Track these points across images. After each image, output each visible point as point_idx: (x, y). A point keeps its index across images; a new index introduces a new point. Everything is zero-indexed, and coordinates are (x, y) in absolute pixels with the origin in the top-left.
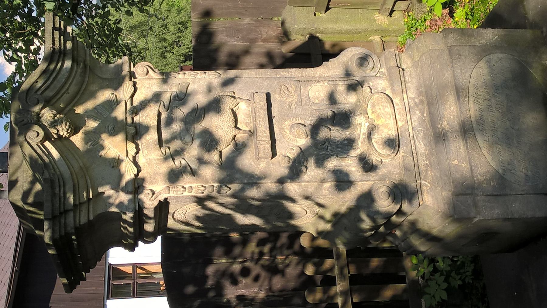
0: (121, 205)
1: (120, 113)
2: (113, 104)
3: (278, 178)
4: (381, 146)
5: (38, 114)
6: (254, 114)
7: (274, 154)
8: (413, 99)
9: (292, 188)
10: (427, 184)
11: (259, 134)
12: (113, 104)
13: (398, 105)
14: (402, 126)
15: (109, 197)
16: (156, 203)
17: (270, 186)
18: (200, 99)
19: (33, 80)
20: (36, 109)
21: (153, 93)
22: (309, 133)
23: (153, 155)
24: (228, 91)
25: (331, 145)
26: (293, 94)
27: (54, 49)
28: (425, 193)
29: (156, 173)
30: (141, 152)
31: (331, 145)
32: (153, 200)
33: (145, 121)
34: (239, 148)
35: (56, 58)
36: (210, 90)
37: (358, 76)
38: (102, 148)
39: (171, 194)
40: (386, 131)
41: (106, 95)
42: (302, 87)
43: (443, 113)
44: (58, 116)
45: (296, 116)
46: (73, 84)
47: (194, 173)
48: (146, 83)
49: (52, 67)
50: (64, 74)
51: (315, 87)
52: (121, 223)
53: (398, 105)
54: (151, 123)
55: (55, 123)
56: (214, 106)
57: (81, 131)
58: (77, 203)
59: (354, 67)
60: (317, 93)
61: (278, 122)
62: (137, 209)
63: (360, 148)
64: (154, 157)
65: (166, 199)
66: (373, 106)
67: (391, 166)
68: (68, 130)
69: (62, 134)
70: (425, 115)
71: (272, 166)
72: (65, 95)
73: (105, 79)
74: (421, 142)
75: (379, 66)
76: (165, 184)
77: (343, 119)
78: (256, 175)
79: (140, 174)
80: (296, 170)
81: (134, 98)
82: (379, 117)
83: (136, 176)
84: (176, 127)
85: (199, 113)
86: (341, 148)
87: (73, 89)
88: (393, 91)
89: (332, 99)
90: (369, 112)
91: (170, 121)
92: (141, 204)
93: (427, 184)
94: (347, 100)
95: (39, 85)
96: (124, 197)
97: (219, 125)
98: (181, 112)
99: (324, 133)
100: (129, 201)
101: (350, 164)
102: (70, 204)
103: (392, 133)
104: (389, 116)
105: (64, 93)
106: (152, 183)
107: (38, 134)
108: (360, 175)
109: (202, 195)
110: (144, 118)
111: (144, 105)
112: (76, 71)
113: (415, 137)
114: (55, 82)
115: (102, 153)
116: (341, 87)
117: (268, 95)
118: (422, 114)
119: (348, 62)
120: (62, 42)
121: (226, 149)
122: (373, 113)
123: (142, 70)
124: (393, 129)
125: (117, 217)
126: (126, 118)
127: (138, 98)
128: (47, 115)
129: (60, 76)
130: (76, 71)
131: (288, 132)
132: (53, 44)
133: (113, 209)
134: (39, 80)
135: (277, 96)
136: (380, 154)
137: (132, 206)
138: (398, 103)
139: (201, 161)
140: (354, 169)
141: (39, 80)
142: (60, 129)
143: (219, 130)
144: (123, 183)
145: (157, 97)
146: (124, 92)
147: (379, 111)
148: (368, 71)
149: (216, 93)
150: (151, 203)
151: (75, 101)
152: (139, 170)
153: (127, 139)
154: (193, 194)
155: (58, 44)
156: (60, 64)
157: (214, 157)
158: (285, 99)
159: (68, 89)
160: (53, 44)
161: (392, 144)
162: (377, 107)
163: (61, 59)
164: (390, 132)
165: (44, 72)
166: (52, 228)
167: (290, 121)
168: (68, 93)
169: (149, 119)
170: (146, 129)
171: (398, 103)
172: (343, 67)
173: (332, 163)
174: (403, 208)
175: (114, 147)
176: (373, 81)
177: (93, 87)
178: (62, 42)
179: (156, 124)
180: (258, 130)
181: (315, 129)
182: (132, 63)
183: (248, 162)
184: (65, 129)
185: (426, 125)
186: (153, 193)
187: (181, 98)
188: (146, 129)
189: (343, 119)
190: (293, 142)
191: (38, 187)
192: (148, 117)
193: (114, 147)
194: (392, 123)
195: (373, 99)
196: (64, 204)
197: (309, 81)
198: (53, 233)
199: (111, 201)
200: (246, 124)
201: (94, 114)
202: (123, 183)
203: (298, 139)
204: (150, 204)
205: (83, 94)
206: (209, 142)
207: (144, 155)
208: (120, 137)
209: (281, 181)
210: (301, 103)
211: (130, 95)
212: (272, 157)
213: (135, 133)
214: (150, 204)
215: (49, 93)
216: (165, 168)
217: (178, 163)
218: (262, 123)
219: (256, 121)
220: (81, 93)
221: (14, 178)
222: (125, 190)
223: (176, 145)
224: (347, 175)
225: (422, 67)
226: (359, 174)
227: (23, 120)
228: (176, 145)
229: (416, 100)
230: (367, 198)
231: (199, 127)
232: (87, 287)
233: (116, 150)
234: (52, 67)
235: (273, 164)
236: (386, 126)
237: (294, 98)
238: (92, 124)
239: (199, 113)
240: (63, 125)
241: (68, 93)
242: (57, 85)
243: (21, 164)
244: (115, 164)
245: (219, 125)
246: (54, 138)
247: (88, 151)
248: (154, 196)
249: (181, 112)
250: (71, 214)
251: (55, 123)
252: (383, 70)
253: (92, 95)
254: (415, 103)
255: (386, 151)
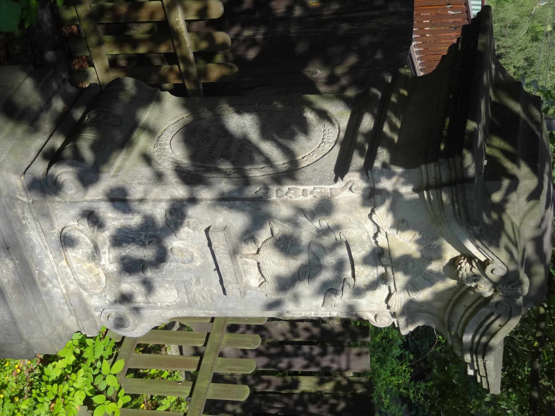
0: (390, 175)
1: (401, 279)
2: (412, 287)
3: (199, 204)
4: (81, 240)
5: (495, 291)
6: (238, 275)
7: (207, 230)
8: (54, 286)
9: (180, 191)
10: (21, 198)
11: (228, 256)
12: (412, 287)
13: (71, 282)
14: (60, 261)
15: (405, 184)
16: (347, 177)
17: (205, 194)
18: (305, 288)
19: (505, 328)
20: (497, 299)
21: (366, 298)
22: (169, 254)
23: (355, 234)
24: (274, 297)
25: (141, 241)
26: (196, 293)
27: (483, 358)
28: (21, 188)
29: (350, 212)
30: (372, 235)
31: (141, 241)
32: (350, 181)
33: (369, 270)
34: (248, 236)
35: (480, 348)
36: (296, 298)
37: (123, 309)
38: (418, 242)
39: (328, 187)
40: (79, 256)
41: (423, 295)
42: (187, 301)
43: (15, 276)
44: (473, 286)
45: (189, 270)
46: (460, 315)
47: (300, 210)
48: (375, 308)
49: (484, 339)
50: (473, 324)
51: (171, 301)
52: (396, 138)
53: (71, 282)
54: (362, 269)
55: (475, 278)
56: (286, 284)
57: (447, 261)
58: (438, 191)
59: (131, 318)
60: (168, 294)
61: (209, 264)
62: (369, 172)
63: (105, 236)
64: (353, 232)
65: (336, 180)
66: (99, 282)
67: (65, 216)
68: (460, 269)
69: (468, 264)
70: (37, 272)
71: (209, 219)
72: (469, 304)
73: (425, 312)
74: (37, 243)
75: (102, 318)
76: (337, 200)
77: (130, 267)
78: (226, 210)
79: (369, 212)
80: (177, 213)
81: (387, 292)
82: (90, 270)
83: (373, 211)
84: (329, 260)
85: (306, 273)
86: (129, 237)
87: (460, 310)
88: (80, 296)
89: (148, 286)
90: (102, 275)
91: (339, 266)
92: (365, 177)
93: (21, 198)
94: (130, 284)
95: (498, 323)
96: (386, 184)
97: (278, 265)
98: (326, 275)
99: (146, 253)
100: (379, 181)
101: (114, 220)
102: (446, 192)
103: (71, 253)
104: (79, 271)
105: (469, 307)
106: (353, 201)
107: (492, 272)
108: (101, 208)
109: (290, 186)
110: (372, 274)
111: (373, 286)
112: (458, 328)
113: (44, 248)
114: (480, 322)
115: (417, 236)
116: (140, 299)
117: (208, 334)
118: (40, 273)
119: (139, 322)
120: (475, 363)
121: (264, 235)
122: (98, 275)
123: (382, 321)
124: (70, 257)
125: (394, 161)
126: (393, 274)
127: (382, 291)
128: (485, 289)
129: (475, 328)
130: (458, 328)
131: (195, 254)
132: (485, 364)
133: (399, 170)
134: (499, 328)
135: (215, 291)
136: (81, 231)
137: (376, 176)
138: (70, 285)
139: (293, 222)
140: (110, 215)
141: (499, 328)
142: (468, 271)
143: (277, 261)
144: (388, 203)
145: (358, 292)
146: (400, 299)
147: (92, 276)
148: (113, 314)
149: (286, 296)
150: (352, 178)
151: (458, 294)
152: (370, 216)
153: (389, 251)
154: (301, 188)
155: (479, 363)
156: (477, 338)
157: (279, 229)
158: (206, 289)
159: (466, 311)
160: (485, 364)
161: (67, 241)
162: (94, 280)
163: (474, 346)
164: (74, 254)
165: (493, 335)
166: (464, 170)
167: (195, 266)
168: (465, 306)
169: (366, 273)
170: (366, 261)
171: (70, 285)
172: (144, 317)
173: (135, 220)
174: (46, 166)
175: (405, 243)
176: (105, 305)
177: (439, 304)
178: (475, 363)
179: (356, 268)
180: (229, 260)
181: (161, 258)
182: (397, 326)
183: (237, 221)
184: (463, 270)
185: (33, 261)
186: (350, 189)
187: (329, 290)
188: (366, 261)
189: (130, 267)
190: (188, 243)
191: (497, 197)
192: (366, 274)
193: (405, 243)
194: (74, 264)
195: (101, 288)
196: (452, 193)
197: (181, 305)
198: (462, 164)
199: (402, 180)
200: (247, 263)
201: (431, 279)
202: (388, 203)
203: (182, 246)
204: (354, 178)
205: (450, 300)
206: (286, 245)
207: (366, 234)
208: (398, 253)
209: (193, 200)
210: (186, 284)
211: (393, 297)
212: (209, 228)
213: (378, 256)
214: (354, 178)
215: (485, 311)
216: (338, 217)
217: (325, 223)
218: (227, 268)
219: (234, 269)
220: (452, 303)
221: (532, 203)
222: (384, 193)
223: (327, 241)
224: (117, 209)
225: (51, 320)
226: (102, 210)
227: (512, 287)
228: (327, 241)
229: (50, 285)
230: (87, 179)
231: (302, 259)
232: (444, 36)
233: (401, 240)
234: (484, 339)
235: (207, 221)
236: (79, 261)
237: (195, 289)
238: (435, 266)
239: (306, 273)
240: (465, 275)
241: (465, 306)
242: (477, 320)
243: (523, 219)
244: (401, 225)
245: (278, 265)
246: (475, 261)
247: (436, 238)
248: (349, 187)
249: (326, 275)
250: (444, 179)
251: (475, 278)
252: (97, 314)
253: (438, 296)
254: (51, 282)
255: (75, 234)
